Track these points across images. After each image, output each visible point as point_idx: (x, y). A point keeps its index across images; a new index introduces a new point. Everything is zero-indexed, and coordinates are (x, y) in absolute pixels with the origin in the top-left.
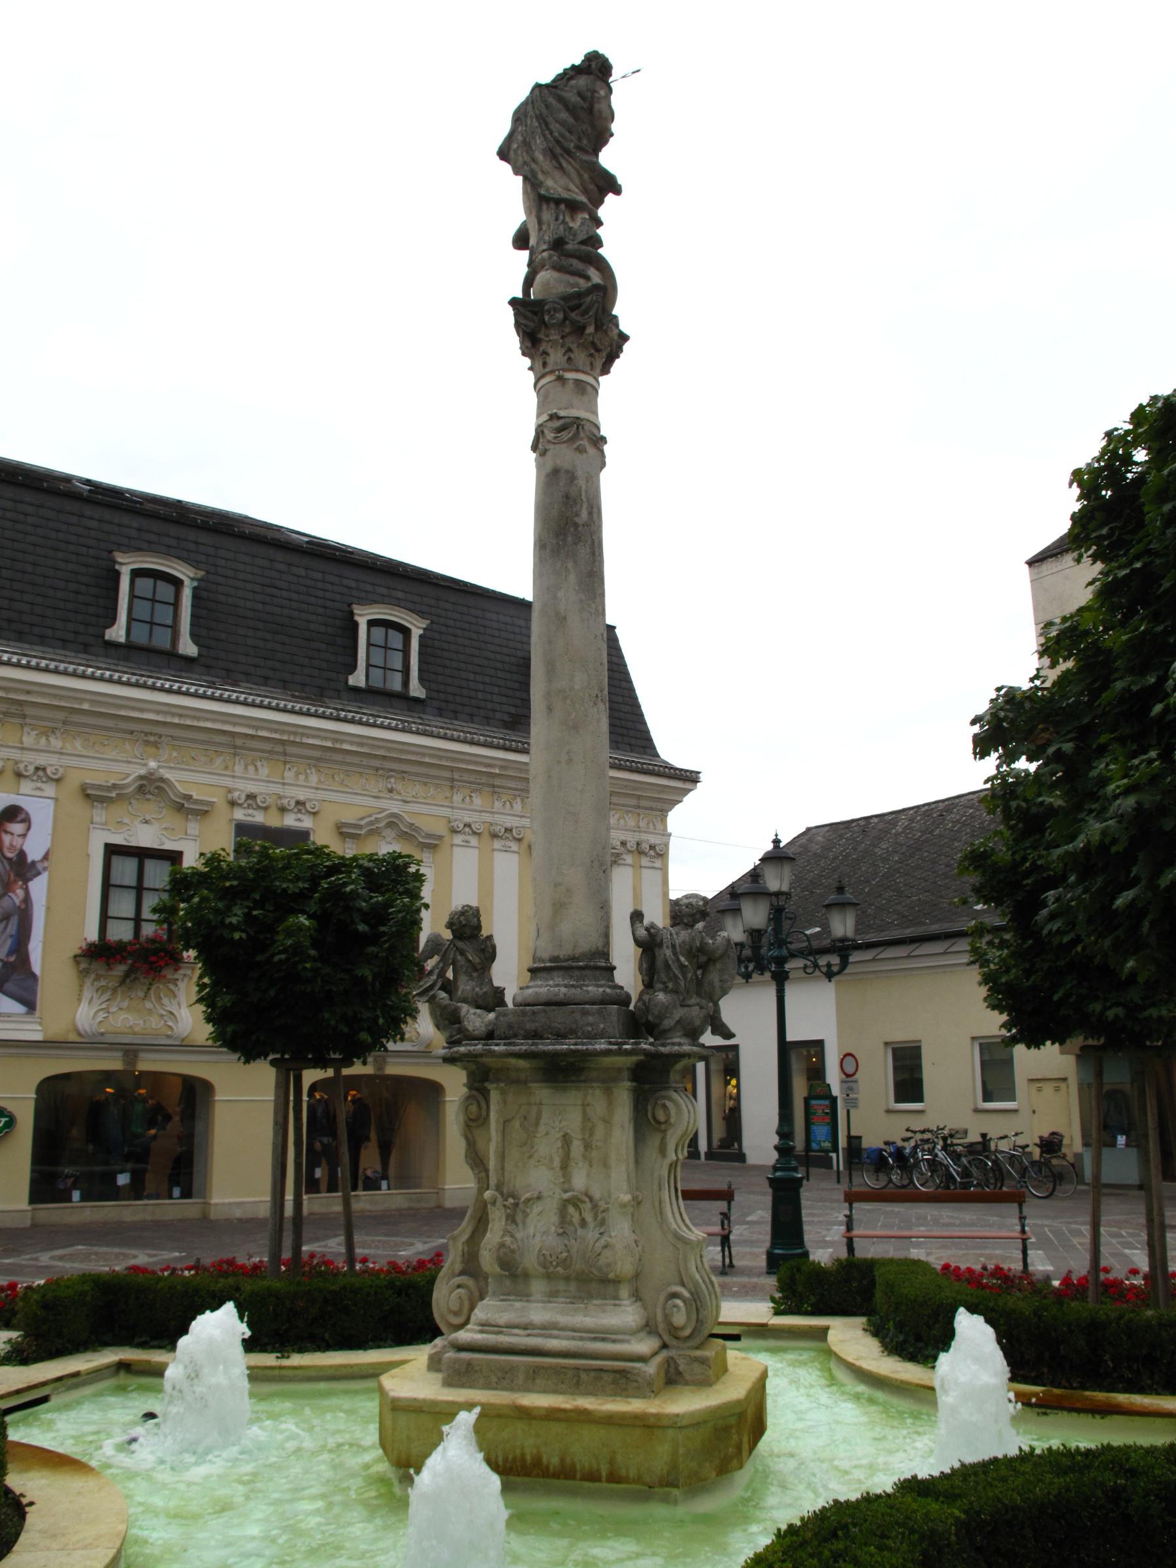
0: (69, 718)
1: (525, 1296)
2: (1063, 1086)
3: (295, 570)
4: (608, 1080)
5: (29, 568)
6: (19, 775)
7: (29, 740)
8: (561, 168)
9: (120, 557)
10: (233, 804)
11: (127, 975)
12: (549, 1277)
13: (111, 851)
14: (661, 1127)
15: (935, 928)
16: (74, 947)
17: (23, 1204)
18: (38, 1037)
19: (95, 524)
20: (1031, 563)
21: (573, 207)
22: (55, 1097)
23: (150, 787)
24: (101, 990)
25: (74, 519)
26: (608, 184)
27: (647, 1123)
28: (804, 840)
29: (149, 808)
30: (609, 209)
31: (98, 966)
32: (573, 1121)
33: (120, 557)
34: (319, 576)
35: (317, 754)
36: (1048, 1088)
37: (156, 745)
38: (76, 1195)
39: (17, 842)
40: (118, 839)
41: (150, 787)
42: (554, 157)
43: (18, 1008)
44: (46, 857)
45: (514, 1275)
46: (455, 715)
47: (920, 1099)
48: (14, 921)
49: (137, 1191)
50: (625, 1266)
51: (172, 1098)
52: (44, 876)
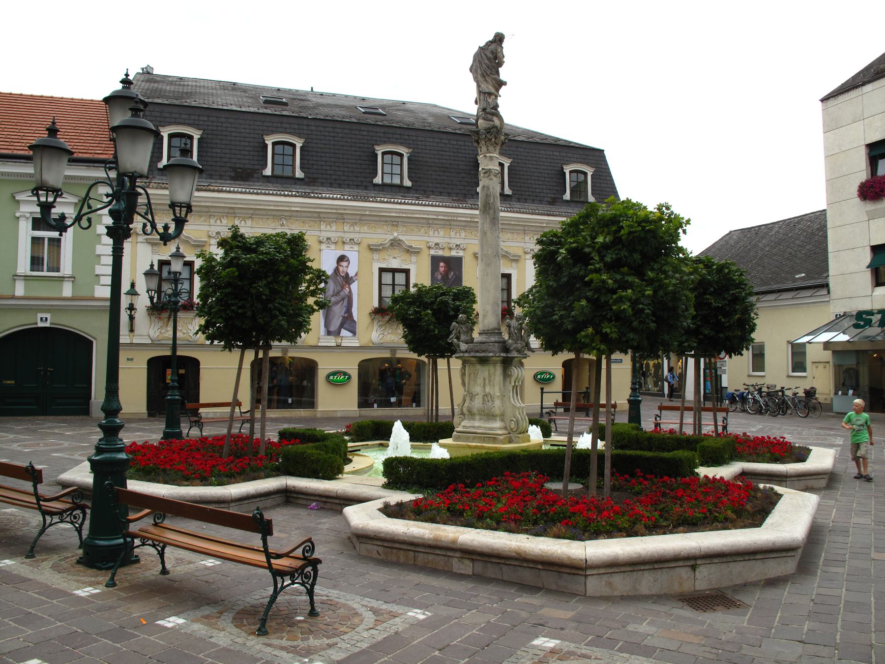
0: (361, 218)
1: (474, 420)
2: (827, 365)
3: (452, 142)
4: (495, 364)
5: (341, 156)
6: (344, 243)
7: (346, 228)
8: (486, 81)
9: (377, 148)
10: (429, 248)
11: (390, 320)
12: (480, 415)
13: (382, 270)
14: (510, 376)
15: (775, 287)
16: (370, 309)
17: (355, 407)
18: (358, 345)
19: (365, 133)
20: (822, 100)
21: (490, 94)
22: (364, 367)
23: (395, 244)
24: (381, 326)
25: (357, 132)
26: (501, 84)
27: (506, 375)
28: (727, 238)
29: (396, 252)
30: (503, 91)
31: (378, 317)
32: (486, 373)
33: (377, 148)
34: (462, 143)
35: (464, 224)
36: (821, 366)
37: (397, 226)
38: (375, 405)
39: (345, 269)
40: (384, 266)
41: (395, 244)
42: (484, 76)
43: (351, 334)
44: (356, 275)
45: (471, 414)
46: (526, 201)
47: (763, 370)
48: (346, 300)
49: (399, 404)
50: (498, 412)
51: (412, 370)
52: (356, 282)
